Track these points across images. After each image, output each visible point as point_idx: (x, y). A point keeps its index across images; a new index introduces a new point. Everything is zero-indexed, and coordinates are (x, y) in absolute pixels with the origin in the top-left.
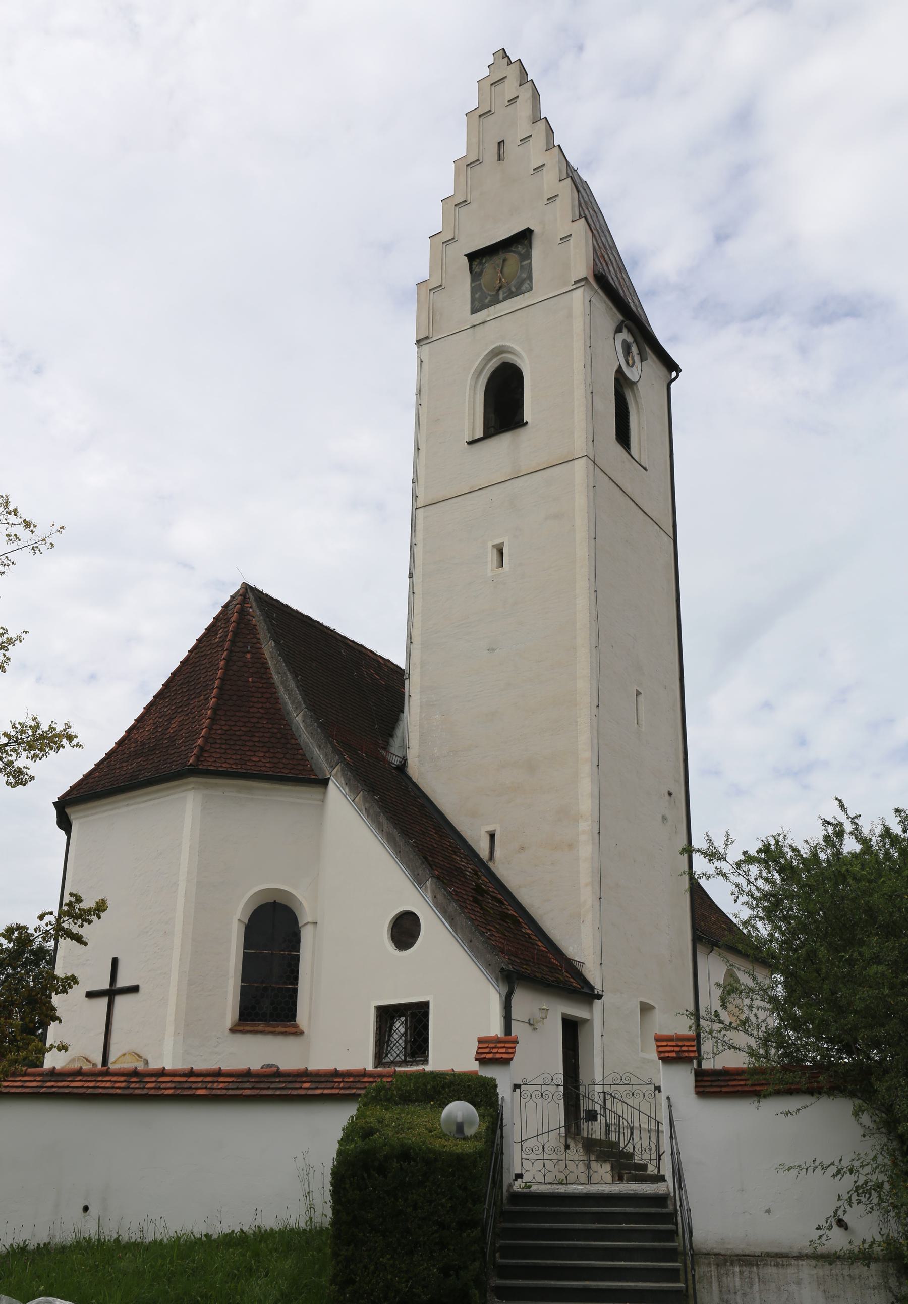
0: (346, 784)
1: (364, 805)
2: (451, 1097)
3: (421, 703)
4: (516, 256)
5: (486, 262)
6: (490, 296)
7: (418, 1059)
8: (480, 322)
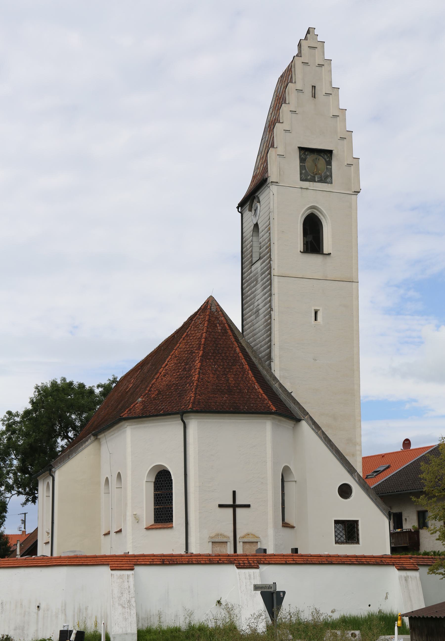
0: (313, 424)
1: (323, 435)
4: (324, 160)
5: (308, 154)
7: (354, 541)
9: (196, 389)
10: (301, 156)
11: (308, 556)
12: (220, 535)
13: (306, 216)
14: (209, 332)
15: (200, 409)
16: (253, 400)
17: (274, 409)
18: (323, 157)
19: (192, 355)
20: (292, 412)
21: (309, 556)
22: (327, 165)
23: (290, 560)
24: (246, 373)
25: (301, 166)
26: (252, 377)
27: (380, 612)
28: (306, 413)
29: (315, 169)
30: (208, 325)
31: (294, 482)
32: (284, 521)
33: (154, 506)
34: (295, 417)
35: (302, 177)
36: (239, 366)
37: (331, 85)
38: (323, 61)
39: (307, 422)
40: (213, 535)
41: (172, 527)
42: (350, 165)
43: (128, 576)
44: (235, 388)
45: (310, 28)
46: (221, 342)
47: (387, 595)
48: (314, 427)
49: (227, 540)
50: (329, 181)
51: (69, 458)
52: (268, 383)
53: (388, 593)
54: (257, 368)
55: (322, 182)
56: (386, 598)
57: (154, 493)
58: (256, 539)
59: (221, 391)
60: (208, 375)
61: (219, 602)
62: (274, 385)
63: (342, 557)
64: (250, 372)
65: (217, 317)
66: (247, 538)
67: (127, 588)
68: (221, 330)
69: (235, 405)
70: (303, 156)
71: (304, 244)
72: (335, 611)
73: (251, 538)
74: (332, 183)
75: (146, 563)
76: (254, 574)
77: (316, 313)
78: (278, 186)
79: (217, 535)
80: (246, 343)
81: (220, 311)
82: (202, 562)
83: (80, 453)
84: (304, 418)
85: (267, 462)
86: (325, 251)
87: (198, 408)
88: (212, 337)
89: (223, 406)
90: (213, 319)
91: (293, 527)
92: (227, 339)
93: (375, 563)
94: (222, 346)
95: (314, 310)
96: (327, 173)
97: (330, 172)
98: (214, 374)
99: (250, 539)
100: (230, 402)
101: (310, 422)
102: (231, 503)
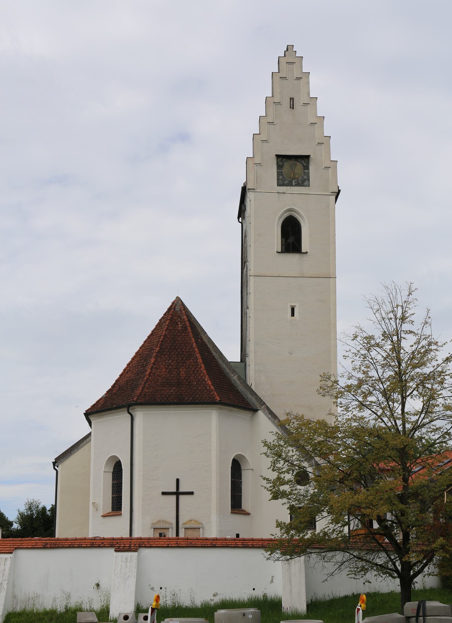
0: (269, 414)
2: (120, 503)
3: (255, 369)
4: (301, 165)
5: (285, 161)
6: (288, 181)
8: (282, 192)
9: (145, 383)
10: (279, 163)
11: (194, 540)
12: (162, 522)
13: (284, 220)
14: (170, 329)
15: (144, 401)
16: (199, 392)
17: (218, 399)
18: (300, 163)
19: (151, 352)
20: (249, 402)
21: (195, 540)
22: (304, 170)
23: (174, 544)
24: (199, 366)
25: (278, 172)
26: (203, 370)
27: (265, 596)
28: (262, 403)
29: (292, 174)
30: (169, 323)
31: (251, 471)
32: (241, 508)
33: (112, 495)
34: (252, 407)
35: (279, 182)
36: (193, 360)
37: (309, 95)
38: (301, 74)
39: (264, 412)
40: (154, 522)
41: (121, 514)
42: (327, 168)
43: (5, 559)
44: (184, 381)
45: (288, 46)
46: (179, 339)
47: (272, 579)
48: (270, 417)
49: (169, 526)
50: (306, 184)
51: (71, 454)
52: (227, 376)
53: (273, 576)
54: (217, 362)
55: (299, 185)
56: (272, 581)
57: (112, 483)
58: (198, 525)
59: (170, 384)
60: (161, 369)
61: (98, 585)
62: (233, 377)
63: (229, 540)
64: (202, 365)
65: (179, 316)
66: (189, 524)
67: (2, 571)
68: (182, 327)
69: (181, 396)
70: (280, 163)
71: (282, 245)
72: (217, 595)
73: (193, 524)
74: (309, 186)
75: (27, 546)
76: (131, 557)
77: (293, 309)
78: (254, 193)
79: (159, 521)
80: (208, 339)
81: (184, 310)
82: (76, 546)
83: (82, 449)
84: (260, 408)
85: (211, 451)
86: (303, 250)
87: (143, 401)
88: (171, 334)
89: (168, 398)
90: (175, 318)
91: (249, 514)
92: (186, 335)
93: (260, 546)
94: (179, 342)
95: (291, 306)
96: (305, 177)
97: (307, 176)
98: (167, 369)
99: (192, 525)
100: (176, 394)
101: (267, 412)
102: (175, 490)
